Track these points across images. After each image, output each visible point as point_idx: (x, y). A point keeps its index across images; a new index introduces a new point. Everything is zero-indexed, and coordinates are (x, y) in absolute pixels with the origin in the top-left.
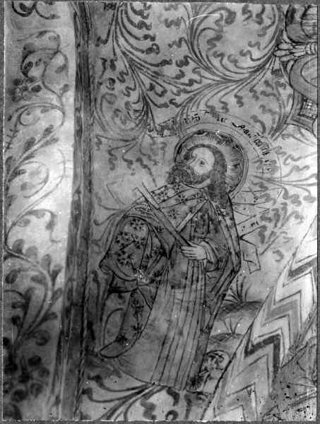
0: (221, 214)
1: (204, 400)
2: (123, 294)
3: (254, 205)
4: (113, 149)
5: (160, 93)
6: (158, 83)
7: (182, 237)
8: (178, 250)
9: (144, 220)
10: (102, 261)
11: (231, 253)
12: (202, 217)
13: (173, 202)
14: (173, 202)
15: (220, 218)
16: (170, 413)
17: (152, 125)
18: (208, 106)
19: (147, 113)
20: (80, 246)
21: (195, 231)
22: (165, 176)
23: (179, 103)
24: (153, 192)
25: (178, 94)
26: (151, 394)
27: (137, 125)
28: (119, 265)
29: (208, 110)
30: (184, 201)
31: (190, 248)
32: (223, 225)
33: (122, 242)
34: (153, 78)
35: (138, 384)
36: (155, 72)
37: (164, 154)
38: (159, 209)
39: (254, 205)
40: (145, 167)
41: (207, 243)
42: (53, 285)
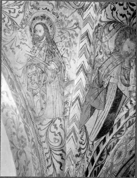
0: (54, 49)
1: (67, 118)
2: (37, 94)
3: (61, 41)
4: (11, 46)
5: (13, 12)
6: (10, 9)
7: (46, 63)
8: (47, 69)
9: (33, 64)
10: (27, 88)
11: (61, 63)
12: (49, 52)
13: (38, 51)
14: (38, 51)
15: (54, 50)
16: (60, 125)
17: (18, 26)
18: (31, 6)
19: (14, 23)
20: (19, 91)
21: (49, 59)
22: (31, 43)
23: (22, 11)
24: (31, 51)
25: (20, 8)
26: (55, 121)
27: (13, 30)
28: (33, 85)
29: (32, 7)
30: (41, 49)
31: (50, 66)
32: (56, 53)
33: (30, 77)
34: (8, 8)
35: (51, 120)
36: (7, 5)
37: (27, 35)
38: (35, 57)
39: (61, 41)
40: (24, 44)
41: (54, 62)
42: (17, 114)
